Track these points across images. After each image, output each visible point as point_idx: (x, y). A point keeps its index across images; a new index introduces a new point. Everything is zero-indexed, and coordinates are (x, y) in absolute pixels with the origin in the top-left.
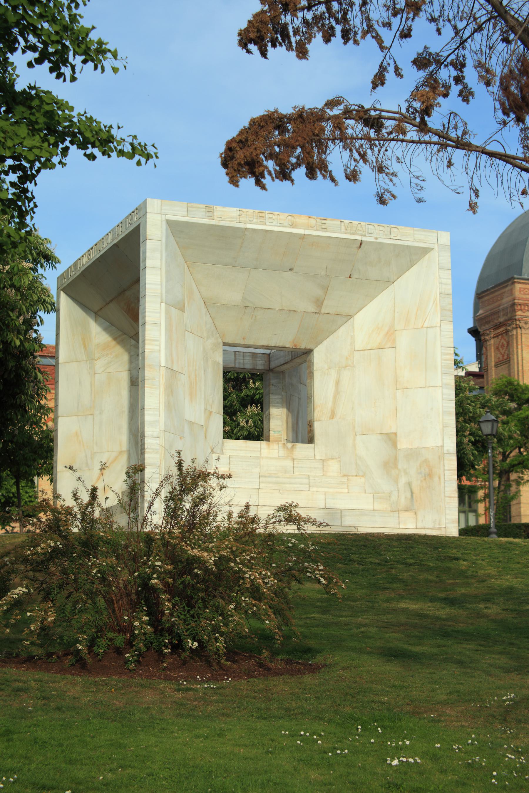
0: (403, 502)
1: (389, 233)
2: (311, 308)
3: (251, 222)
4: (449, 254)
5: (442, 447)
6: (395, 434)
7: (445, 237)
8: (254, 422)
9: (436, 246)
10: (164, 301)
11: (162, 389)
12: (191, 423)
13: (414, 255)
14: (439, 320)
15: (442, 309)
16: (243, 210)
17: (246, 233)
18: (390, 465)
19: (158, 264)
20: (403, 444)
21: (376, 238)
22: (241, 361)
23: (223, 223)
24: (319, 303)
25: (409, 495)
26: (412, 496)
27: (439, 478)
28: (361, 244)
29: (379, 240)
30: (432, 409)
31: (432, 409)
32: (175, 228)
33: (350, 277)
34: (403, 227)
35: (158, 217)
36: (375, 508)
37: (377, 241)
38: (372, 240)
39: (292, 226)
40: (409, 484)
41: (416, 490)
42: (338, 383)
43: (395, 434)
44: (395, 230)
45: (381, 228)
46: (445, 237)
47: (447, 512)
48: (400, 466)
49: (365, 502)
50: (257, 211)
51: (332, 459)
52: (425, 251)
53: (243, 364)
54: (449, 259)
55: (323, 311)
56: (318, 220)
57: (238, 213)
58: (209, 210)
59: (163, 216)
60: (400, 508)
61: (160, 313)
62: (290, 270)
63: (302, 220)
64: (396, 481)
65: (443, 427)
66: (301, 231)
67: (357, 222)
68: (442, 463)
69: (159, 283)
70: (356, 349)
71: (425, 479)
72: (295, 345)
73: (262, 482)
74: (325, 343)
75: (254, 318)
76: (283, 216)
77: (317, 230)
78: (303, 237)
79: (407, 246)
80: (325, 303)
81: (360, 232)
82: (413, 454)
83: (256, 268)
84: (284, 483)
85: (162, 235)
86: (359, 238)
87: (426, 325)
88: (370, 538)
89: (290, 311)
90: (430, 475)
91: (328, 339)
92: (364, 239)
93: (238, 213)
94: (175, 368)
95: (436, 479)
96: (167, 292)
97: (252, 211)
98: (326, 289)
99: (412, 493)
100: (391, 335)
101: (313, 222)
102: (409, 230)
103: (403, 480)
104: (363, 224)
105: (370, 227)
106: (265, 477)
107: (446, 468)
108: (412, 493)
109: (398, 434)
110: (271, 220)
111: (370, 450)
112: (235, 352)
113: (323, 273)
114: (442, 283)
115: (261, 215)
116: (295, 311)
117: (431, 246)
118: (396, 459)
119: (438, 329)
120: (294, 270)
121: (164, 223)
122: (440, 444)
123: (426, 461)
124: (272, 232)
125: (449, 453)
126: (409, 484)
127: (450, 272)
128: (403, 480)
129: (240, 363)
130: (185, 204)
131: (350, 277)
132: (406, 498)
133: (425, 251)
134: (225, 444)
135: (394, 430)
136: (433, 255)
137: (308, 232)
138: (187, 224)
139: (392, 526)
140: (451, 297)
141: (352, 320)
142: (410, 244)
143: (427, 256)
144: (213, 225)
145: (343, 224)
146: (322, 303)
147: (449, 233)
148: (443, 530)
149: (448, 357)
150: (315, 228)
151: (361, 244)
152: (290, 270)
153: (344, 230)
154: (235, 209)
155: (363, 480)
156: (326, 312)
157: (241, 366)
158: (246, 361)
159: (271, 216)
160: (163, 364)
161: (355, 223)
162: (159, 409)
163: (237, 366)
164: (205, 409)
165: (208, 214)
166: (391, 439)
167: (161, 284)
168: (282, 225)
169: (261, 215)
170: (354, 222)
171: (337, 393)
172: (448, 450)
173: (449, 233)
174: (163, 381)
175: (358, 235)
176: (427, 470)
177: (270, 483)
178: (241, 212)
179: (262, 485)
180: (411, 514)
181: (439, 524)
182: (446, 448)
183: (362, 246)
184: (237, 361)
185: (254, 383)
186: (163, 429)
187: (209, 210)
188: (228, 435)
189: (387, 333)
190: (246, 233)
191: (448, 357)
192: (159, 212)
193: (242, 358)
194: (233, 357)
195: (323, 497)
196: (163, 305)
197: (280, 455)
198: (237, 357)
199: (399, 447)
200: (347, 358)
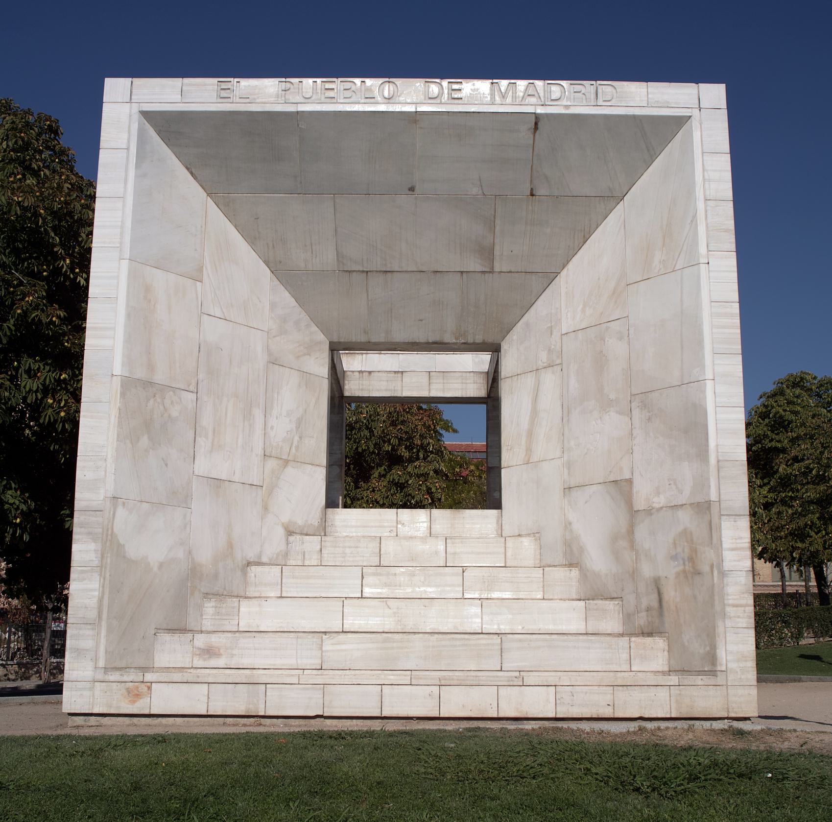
2: (474, 264)
13: (655, 135)
21: (567, 107)
24: (487, 253)
33: (532, 195)
52: (680, 122)
55: (497, 268)
94: (160, 377)
105: (554, 88)
113: (475, 190)
114: (709, 181)
120: (417, 189)
121: (136, 116)
151: (536, 124)
189: (613, 293)
196: (125, 264)
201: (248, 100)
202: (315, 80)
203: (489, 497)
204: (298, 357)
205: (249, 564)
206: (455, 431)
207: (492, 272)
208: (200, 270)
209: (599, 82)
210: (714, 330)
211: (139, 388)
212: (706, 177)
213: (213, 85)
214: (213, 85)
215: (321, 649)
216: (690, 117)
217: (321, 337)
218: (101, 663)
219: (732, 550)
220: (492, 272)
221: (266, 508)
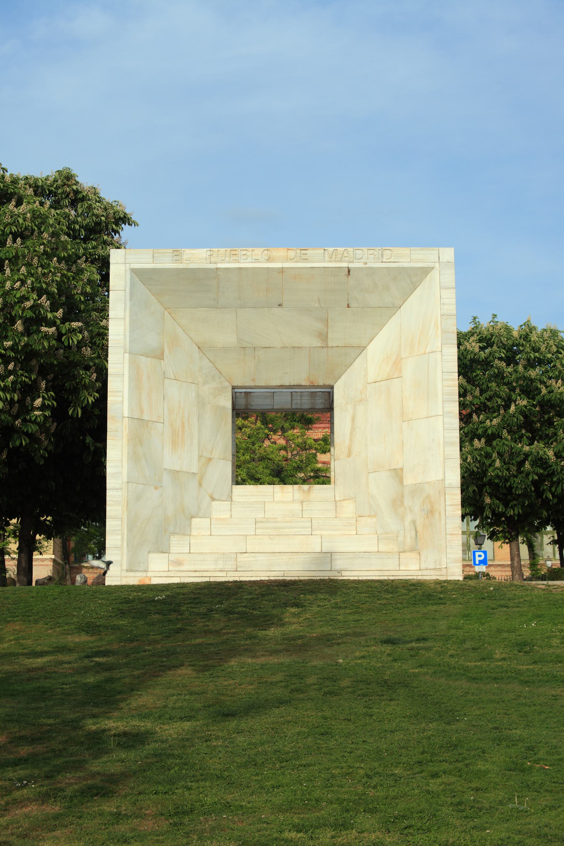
0: (409, 542)
1: (380, 256)
2: (317, 343)
3: (223, 261)
4: (453, 271)
5: (443, 480)
6: (402, 469)
7: (448, 254)
8: (473, 458)
9: (437, 265)
10: (128, 351)
11: (125, 441)
12: (175, 473)
13: (415, 277)
14: (440, 345)
15: (444, 332)
16: (214, 250)
17: (218, 273)
18: (397, 503)
19: (121, 315)
20: (409, 480)
21: (366, 263)
22: (299, 402)
23: (191, 266)
24: (323, 337)
25: (414, 535)
26: (416, 535)
27: (440, 514)
28: (349, 271)
29: (368, 265)
30: (433, 440)
31: (433, 440)
32: (141, 275)
33: (348, 307)
34: (395, 248)
35: (122, 267)
36: (380, 550)
37: (367, 266)
38: (361, 265)
39: (269, 260)
40: (414, 522)
41: (420, 529)
42: (353, 419)
43: (402, 469)
44: (389, 252)
45: (371, 252)
46: (448, 254)
47: (449, 550)
48: (406, 504)
49: (368, 544)
50: (229, 249)
51: (349, 499)
52: (426, 271)
53: (301, 404)
54: (453, 277)
55: (330, 344)
56: (298, 251)
57: (209, 253)
58: (177, 254)
59: (128, 265)
60: (406, 548)
61: (123, 363)
62: (279, 305)
63: (280, 253)
64: (403, 520)
65: (445, 459)
66: (278, 265)
67: (343, 249)
68: (443, 498)
69: (123, 333)
70: (369, 382)
71: (427, 516)
72: (312, 383)
73: (259, 528)
74: (343, 377)
75: (256, 358)
76: (258, 251)
77: (296, 262)
78: (282, 271)
79: (403, 268)
80: (330, 335)
81: (347, 259)
82: (417, 489)
83: (242, 307)
84: (284, 528)
85: (125, 285)
86: (345, 265)
87: (427, 351)
88: (142, 588)
89: (294, 347)
90: (431, 512)
91: (345, 374)
92: (351, 265)
93: (209, 253)
94: (146, 417)
95: (437, 515)
96: (131, 342)
97: (224, 250)
98: (326, 322)
99: (416, 532)
100: (397, 364)
101: (292, 254)
102: (405, 251)
103: (409, 518)
104: (350, 249)
105: (358, 252)
106: (262, 522)
107: (447, 503)
108: (416, 532)
109: (404, 469)
110: (245, 257)
111: (379, 487)
112: (292, 392)
113: (317, 305)
114: (443, 304)
115: (233, 252)
116: (299, 347)
117: (431, 265)
118: (402, 496)
119: (439, 354)
120: (284, 305)
121: (128, 272)
122: (441, 477)
123: (428, 497)
124: (246, 269)
125: (451, 487)
126: (414, 522)
127: (454, 291)
128: (409, 518)
129: (297, 404)
130: (151, 251)
131: (348, 307)
132: (411, 537)
133: (426, 271)
134: (234, 490)
135: (400, 466)
136: (435, 274)
137: (286, 265)
138: (153, 271)
139: (391, 568)
140: (455, 317)
141: (365, 350)
142: (406, 265)
143: (429, 276)
144: (181, 269)
145: (326, 252)
146: (327, 337)
147: (453, 249)
148: (444, 572)
149: (451, 383)
150: (294, 260)
151: (349, 271)
152: (279, 305)
153: (327, 259)
154: (205, 250)
155: (374, 520)
156: (334, 345)
157: (299, 407)
158: (303, 401)
159: (244, 252)
160: (126, 414)
161: (341, 249)
162: (122, 460)
163: (294, 407)
164: (200, 457)
165: (176, 258)
166: (398, 474)
167: (125, 335)
168: (257, 261)
169: (233, 252)
170: (339, 249)
171: (353, 429)
172: (449, 484)
173: (453, 249)
174: (126, 432)
175: (345, 262)
176: (429, 506)
177: (267, 528)
178: (212, 253)
179: (258, 531)
180: (414, 555)
181: (440, 565)
182: (447, 482)
183: (351, 273)
184: (294, 402)
185: (478, 417)
186: (125, 480)
187: (177, 254)
188: (238, 481)
189: (395, 362)
190: (218, 273)
191: (451, 383)
192: (123, 261)
193: (299, 398)
194: (290, 398)
195: (319, 540)
196: (127, 355)
197: (295, 498)
198: (294, 398)
199: (405, 483)
200: (361, 392)
201: (189, 262)
202: (226, 249)
203: (321, 477)
204: (215, 397)
205: (192, 517)
206: (495, 316)
207: (327, 347)
208: (163, 354)
209: (383, 248)
210: (444, 388)
211: (140, 425)
212: (442, 302)
213: (170, 253)
214: (170, 253)
215: (236, 560)
216: (433, 268)
217: (227, 384)
218: (125, 567)
219: (451, 505)
220: (327, 347)
221: (200, 485)
